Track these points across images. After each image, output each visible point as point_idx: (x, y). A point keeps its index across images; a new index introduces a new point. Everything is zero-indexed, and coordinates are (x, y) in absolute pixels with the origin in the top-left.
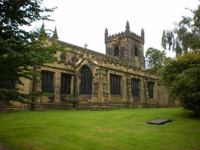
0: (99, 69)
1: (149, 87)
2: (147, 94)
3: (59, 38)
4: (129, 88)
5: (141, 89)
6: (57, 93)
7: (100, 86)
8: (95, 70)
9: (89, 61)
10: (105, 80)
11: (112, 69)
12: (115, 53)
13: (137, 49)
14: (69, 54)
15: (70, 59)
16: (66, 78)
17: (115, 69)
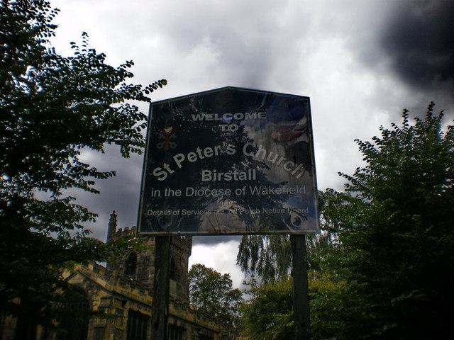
0: (109, 298)
7: (107, 335)
10: (119, 322)
11: (133, 301)
12: (128, 267)
13: (174, 265)
17: (140, 300)
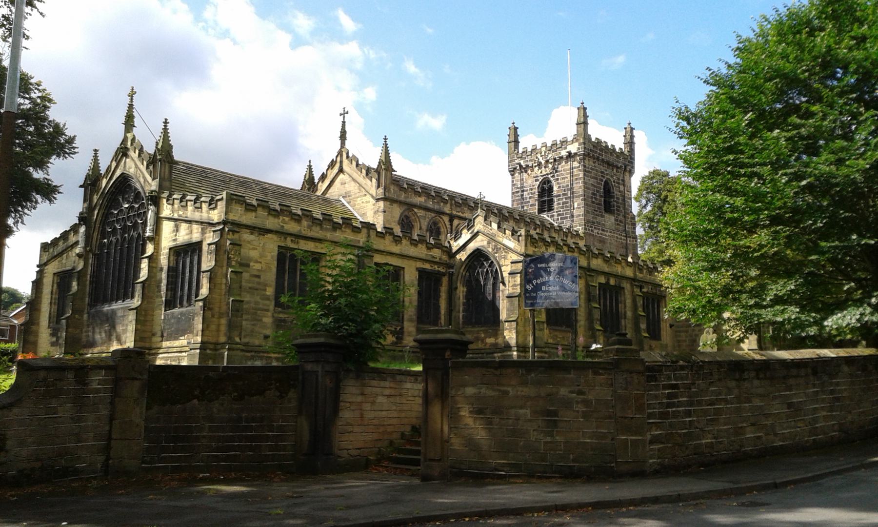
1: (648, 309)
2: (643, 326)
3: (28, 38)
4: (638, 298)
5: (625, 312)
6: (410, 320)
8: (508, 262)
9: (491, 239)
14: (421, 213)
15: (424, 227)
16: (429, 281)
